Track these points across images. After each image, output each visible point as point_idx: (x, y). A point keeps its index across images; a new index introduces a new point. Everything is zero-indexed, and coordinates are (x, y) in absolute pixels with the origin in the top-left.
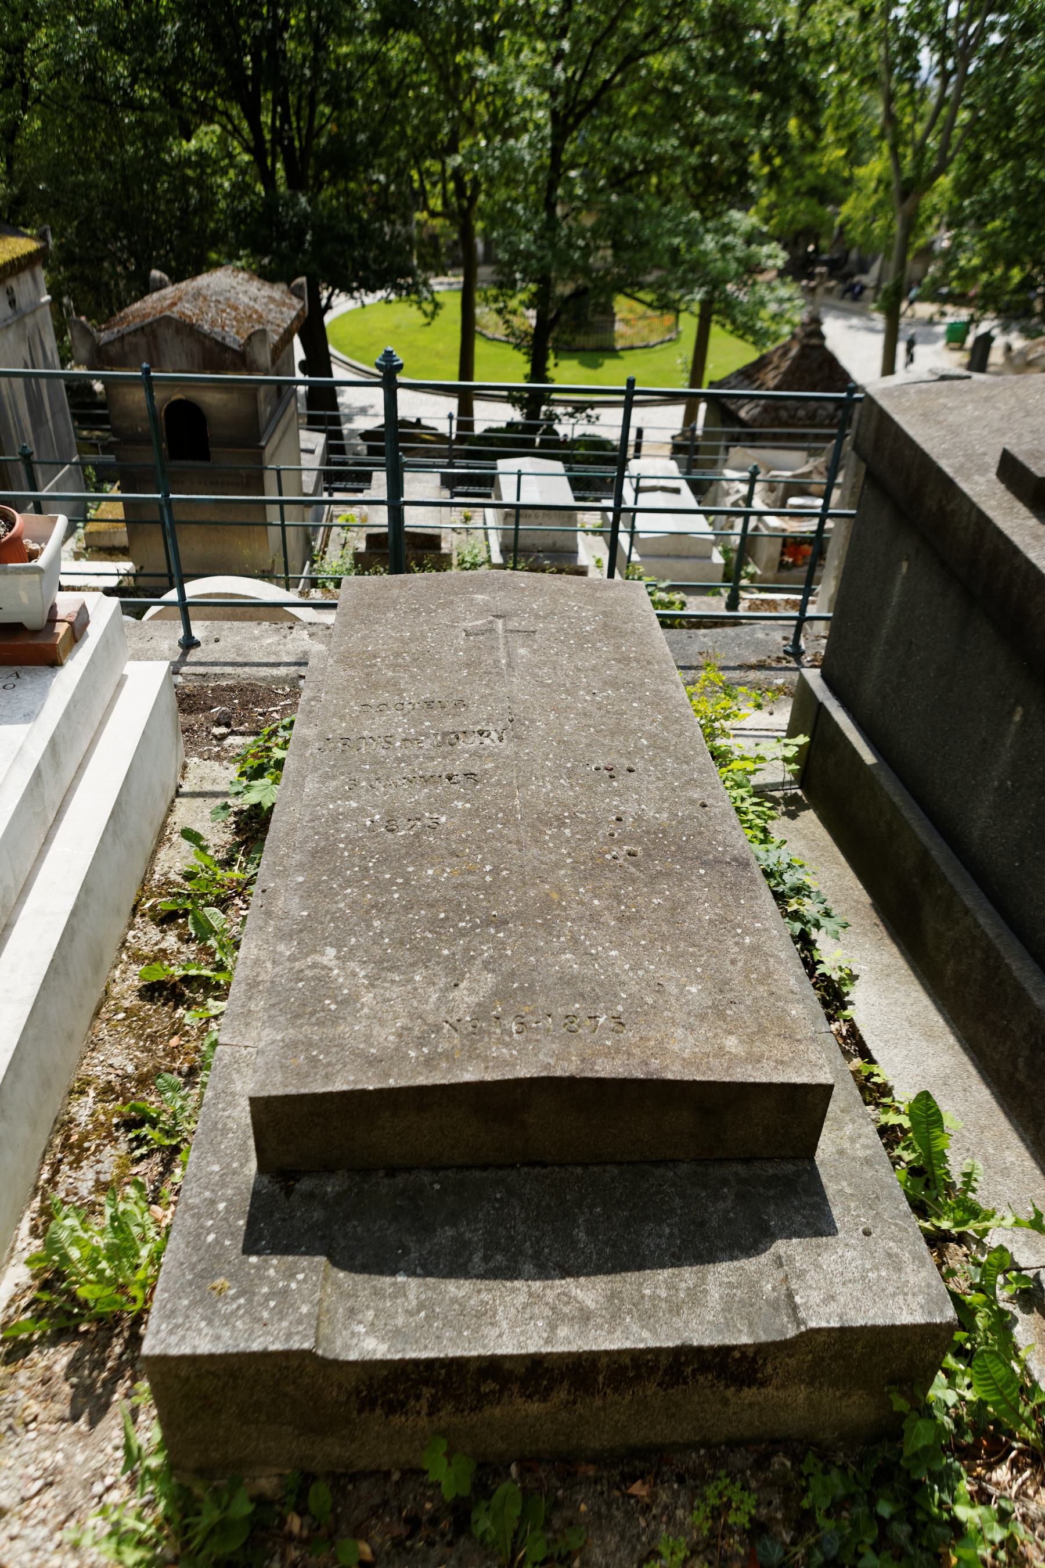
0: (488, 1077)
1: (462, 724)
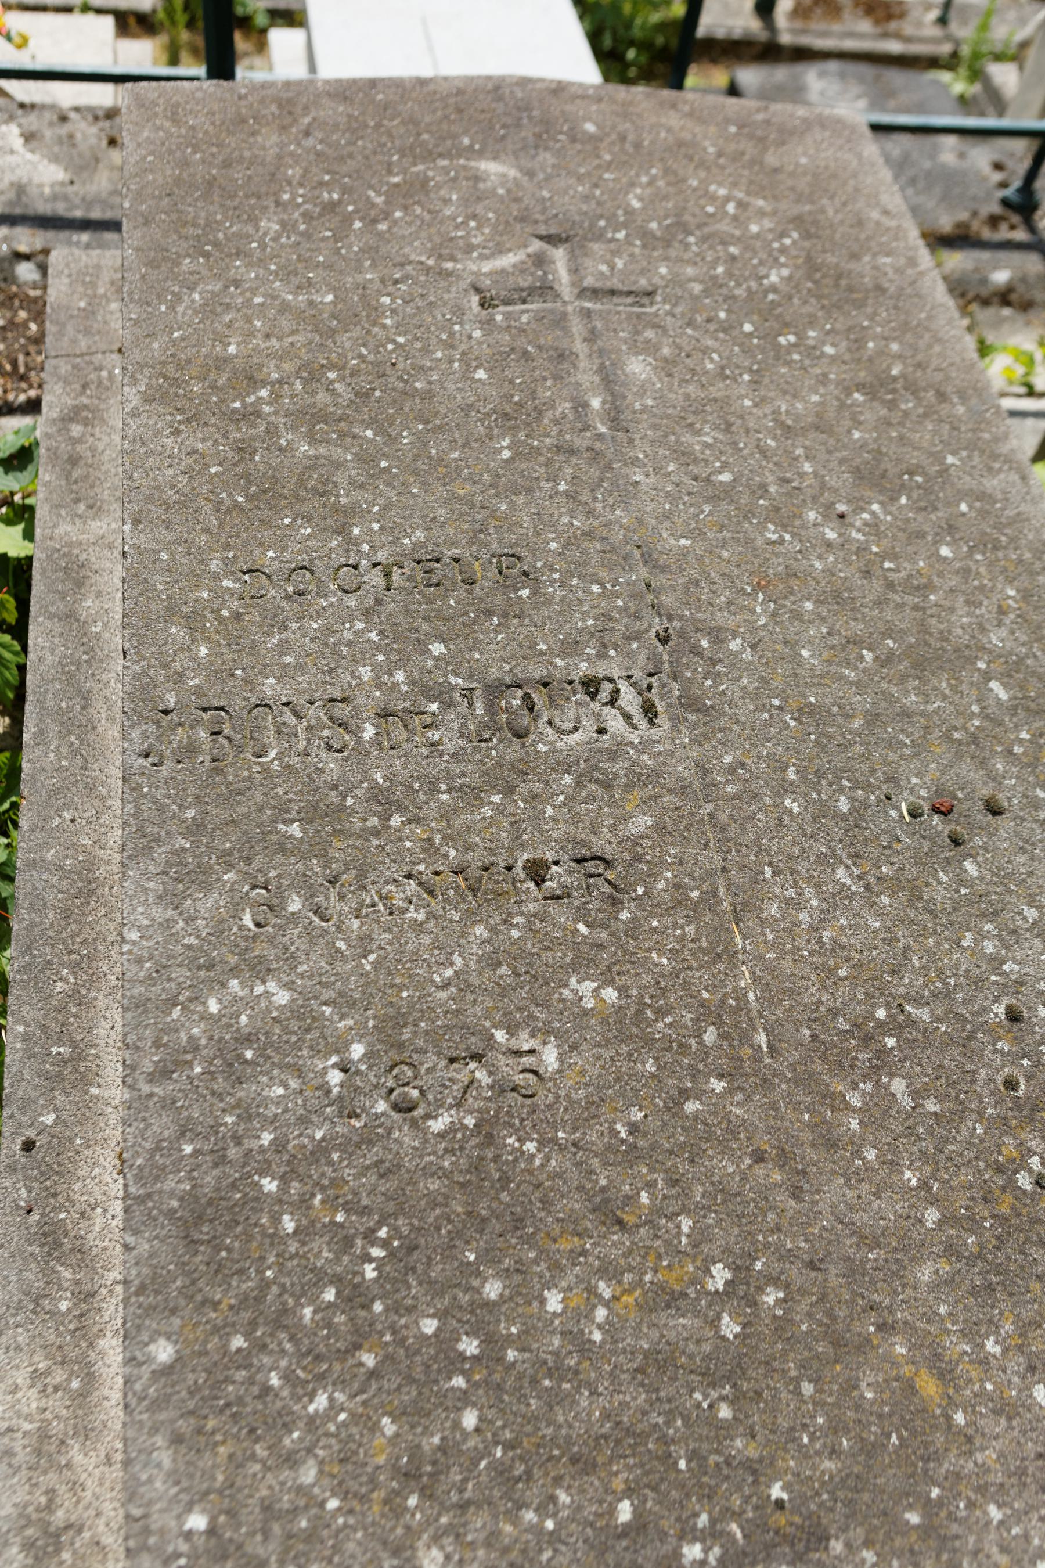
1: (530, 652)
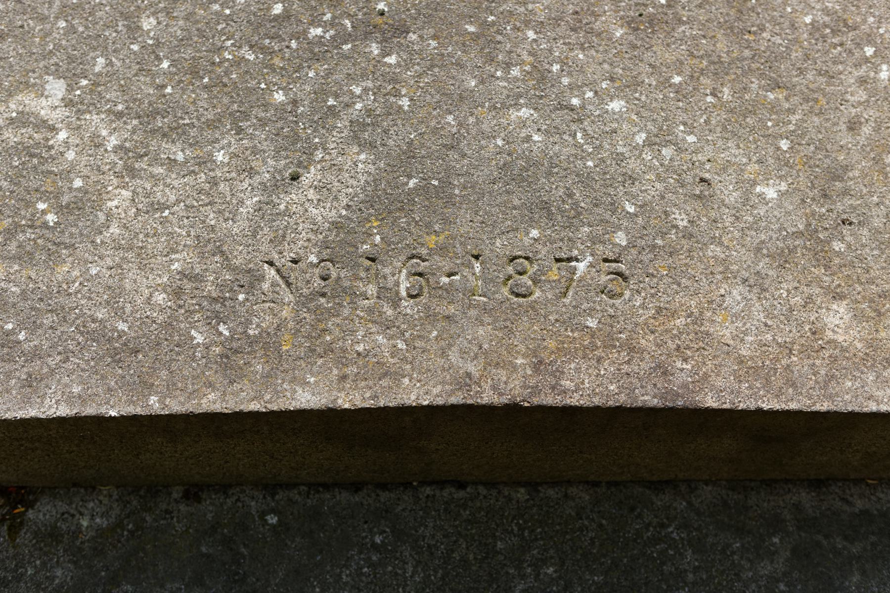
0: (347, 399)
